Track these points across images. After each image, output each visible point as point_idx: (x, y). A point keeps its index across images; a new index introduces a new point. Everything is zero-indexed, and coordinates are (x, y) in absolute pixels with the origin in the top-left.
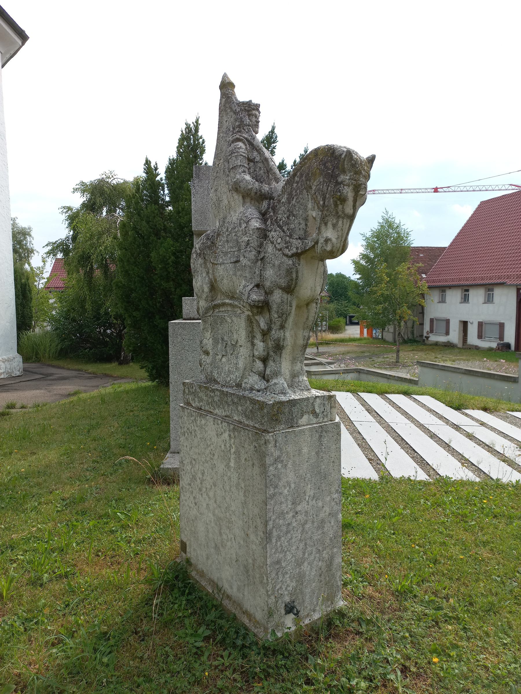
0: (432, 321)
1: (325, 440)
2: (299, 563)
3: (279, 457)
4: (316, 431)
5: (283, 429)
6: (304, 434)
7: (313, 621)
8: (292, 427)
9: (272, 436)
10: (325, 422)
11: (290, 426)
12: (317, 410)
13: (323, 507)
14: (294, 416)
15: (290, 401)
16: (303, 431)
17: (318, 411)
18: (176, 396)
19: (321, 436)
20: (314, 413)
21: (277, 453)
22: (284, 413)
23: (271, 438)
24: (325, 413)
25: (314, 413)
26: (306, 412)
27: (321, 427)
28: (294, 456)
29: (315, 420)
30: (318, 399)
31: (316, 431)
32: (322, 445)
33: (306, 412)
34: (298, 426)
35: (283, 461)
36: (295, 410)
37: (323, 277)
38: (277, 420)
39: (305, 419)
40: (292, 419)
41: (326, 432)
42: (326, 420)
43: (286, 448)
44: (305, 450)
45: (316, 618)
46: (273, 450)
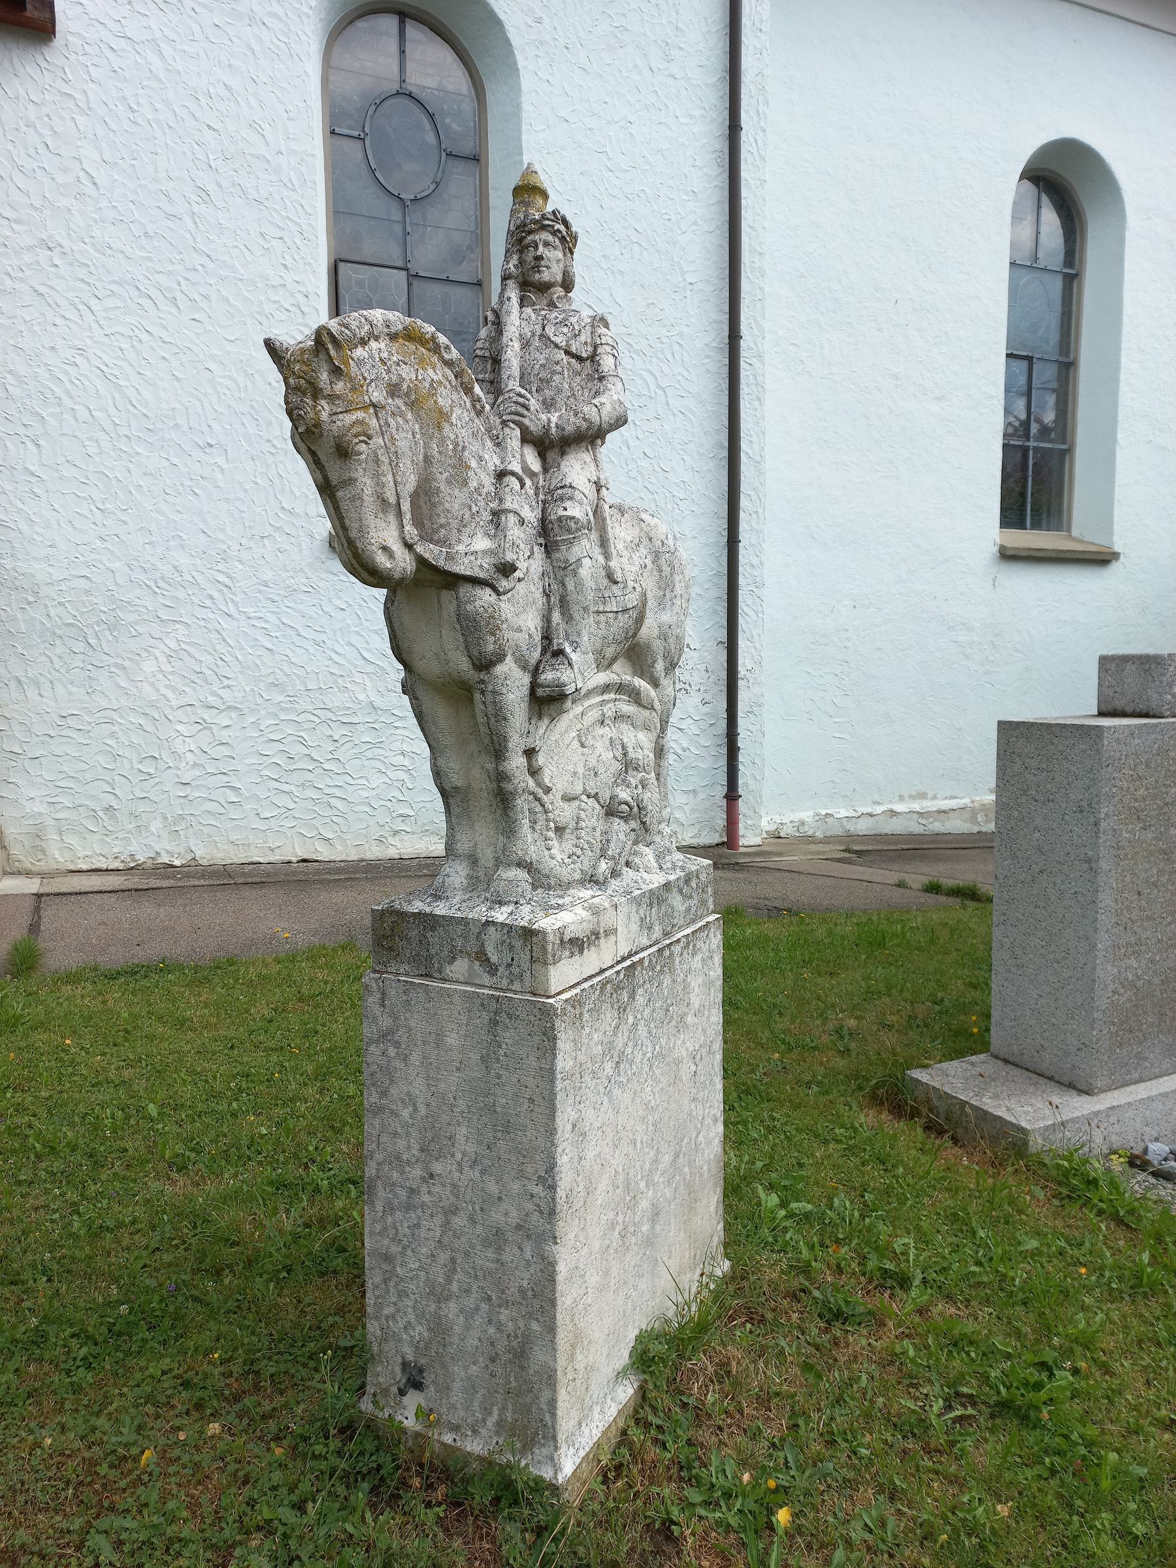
0: (1101, 714)
1: (507, 1037)
2: (440, 1295)
3: (391, 1032)
4: (482, 1005)
5: (407, 975)
6: (451, 1003)
7: (458, 1449)
8: (428, 976)
9: (376, 980)
10: (515, 992)
11: (423, 971)
12: (490, 955)
13: (500, 1199)
14: (433, 952)
15: (420, 915)
16: (449, 994)
17: (494, 959)
18: (1004, 914)
19: (494, 1023)
20: (481, 957)
21: (386, 1022)
22: (408, 940)
23: (374, 985)
24: (514, 969)
25: (481, 957)
26: (461, 951)
27: (497, 999)
28: (424, 1043)
29: (486, 979)
30: (492, 929)
31: (482, 1005)
32: (500, 1046)
33: (461, 951)
34: (444, 980)
35: (397, 1042)
36: (433, 938)
37: (458, 627)
38: (391, 949)
39: (460, 967)
40: (430, 958)
41: (510, 1016)
42: (517, 986)
43: (406, 1019)
44: (452, 1040)
45: (469, 1449)
46: (377, 1011)
